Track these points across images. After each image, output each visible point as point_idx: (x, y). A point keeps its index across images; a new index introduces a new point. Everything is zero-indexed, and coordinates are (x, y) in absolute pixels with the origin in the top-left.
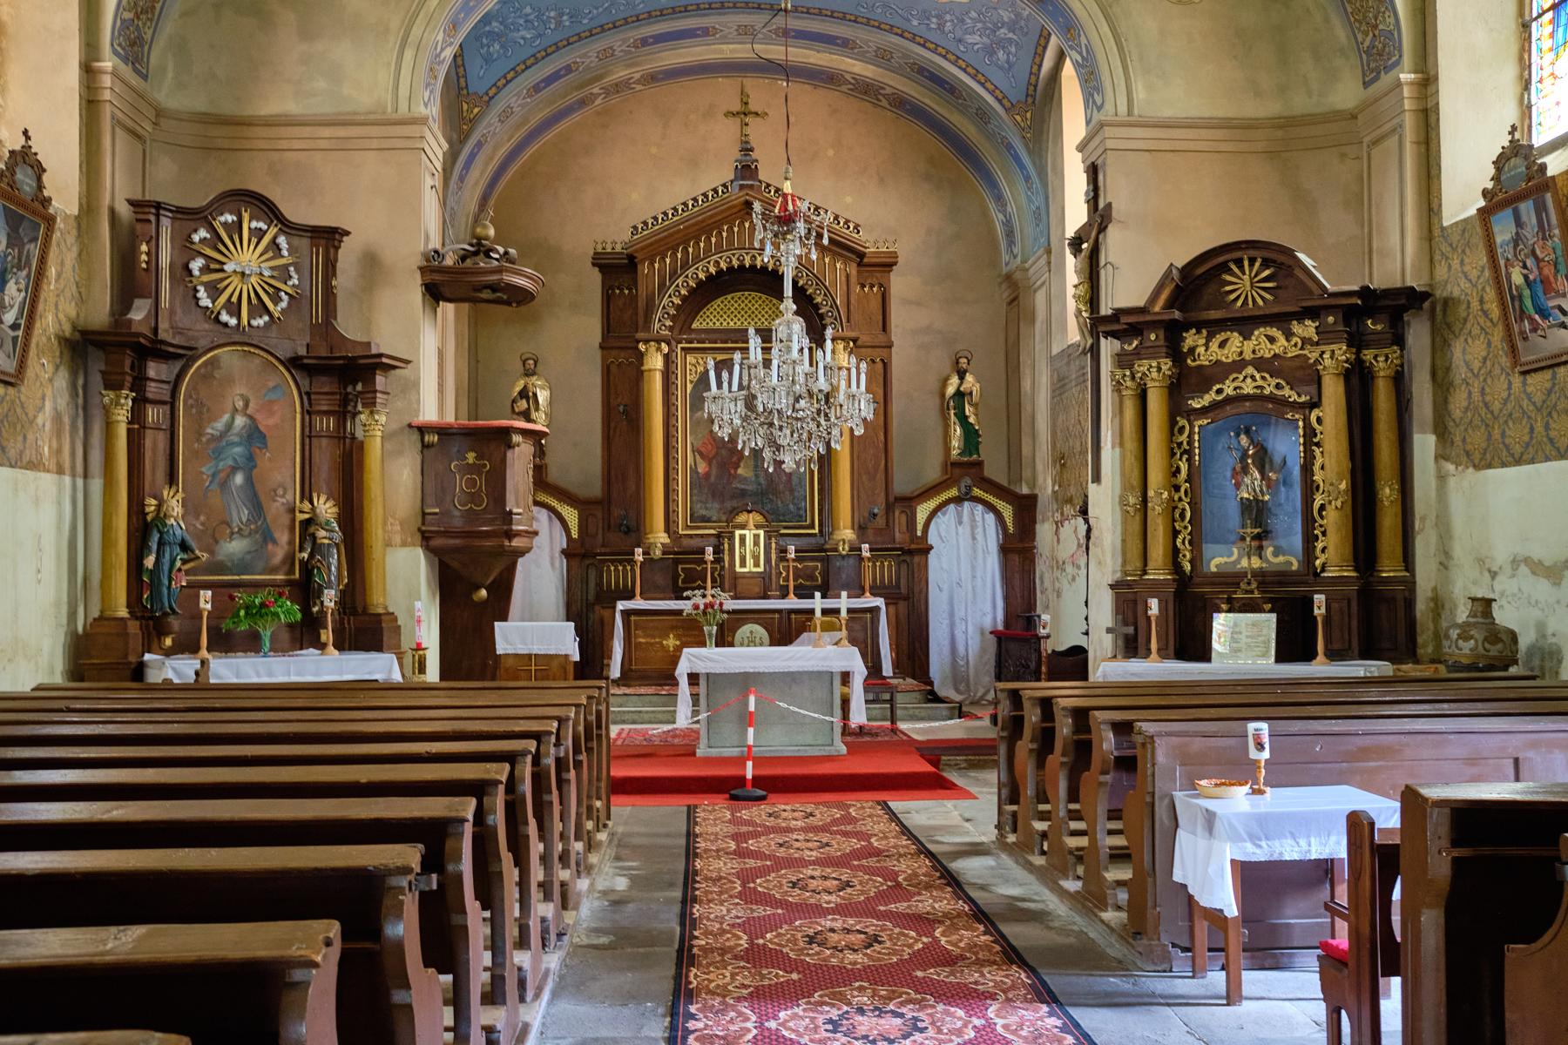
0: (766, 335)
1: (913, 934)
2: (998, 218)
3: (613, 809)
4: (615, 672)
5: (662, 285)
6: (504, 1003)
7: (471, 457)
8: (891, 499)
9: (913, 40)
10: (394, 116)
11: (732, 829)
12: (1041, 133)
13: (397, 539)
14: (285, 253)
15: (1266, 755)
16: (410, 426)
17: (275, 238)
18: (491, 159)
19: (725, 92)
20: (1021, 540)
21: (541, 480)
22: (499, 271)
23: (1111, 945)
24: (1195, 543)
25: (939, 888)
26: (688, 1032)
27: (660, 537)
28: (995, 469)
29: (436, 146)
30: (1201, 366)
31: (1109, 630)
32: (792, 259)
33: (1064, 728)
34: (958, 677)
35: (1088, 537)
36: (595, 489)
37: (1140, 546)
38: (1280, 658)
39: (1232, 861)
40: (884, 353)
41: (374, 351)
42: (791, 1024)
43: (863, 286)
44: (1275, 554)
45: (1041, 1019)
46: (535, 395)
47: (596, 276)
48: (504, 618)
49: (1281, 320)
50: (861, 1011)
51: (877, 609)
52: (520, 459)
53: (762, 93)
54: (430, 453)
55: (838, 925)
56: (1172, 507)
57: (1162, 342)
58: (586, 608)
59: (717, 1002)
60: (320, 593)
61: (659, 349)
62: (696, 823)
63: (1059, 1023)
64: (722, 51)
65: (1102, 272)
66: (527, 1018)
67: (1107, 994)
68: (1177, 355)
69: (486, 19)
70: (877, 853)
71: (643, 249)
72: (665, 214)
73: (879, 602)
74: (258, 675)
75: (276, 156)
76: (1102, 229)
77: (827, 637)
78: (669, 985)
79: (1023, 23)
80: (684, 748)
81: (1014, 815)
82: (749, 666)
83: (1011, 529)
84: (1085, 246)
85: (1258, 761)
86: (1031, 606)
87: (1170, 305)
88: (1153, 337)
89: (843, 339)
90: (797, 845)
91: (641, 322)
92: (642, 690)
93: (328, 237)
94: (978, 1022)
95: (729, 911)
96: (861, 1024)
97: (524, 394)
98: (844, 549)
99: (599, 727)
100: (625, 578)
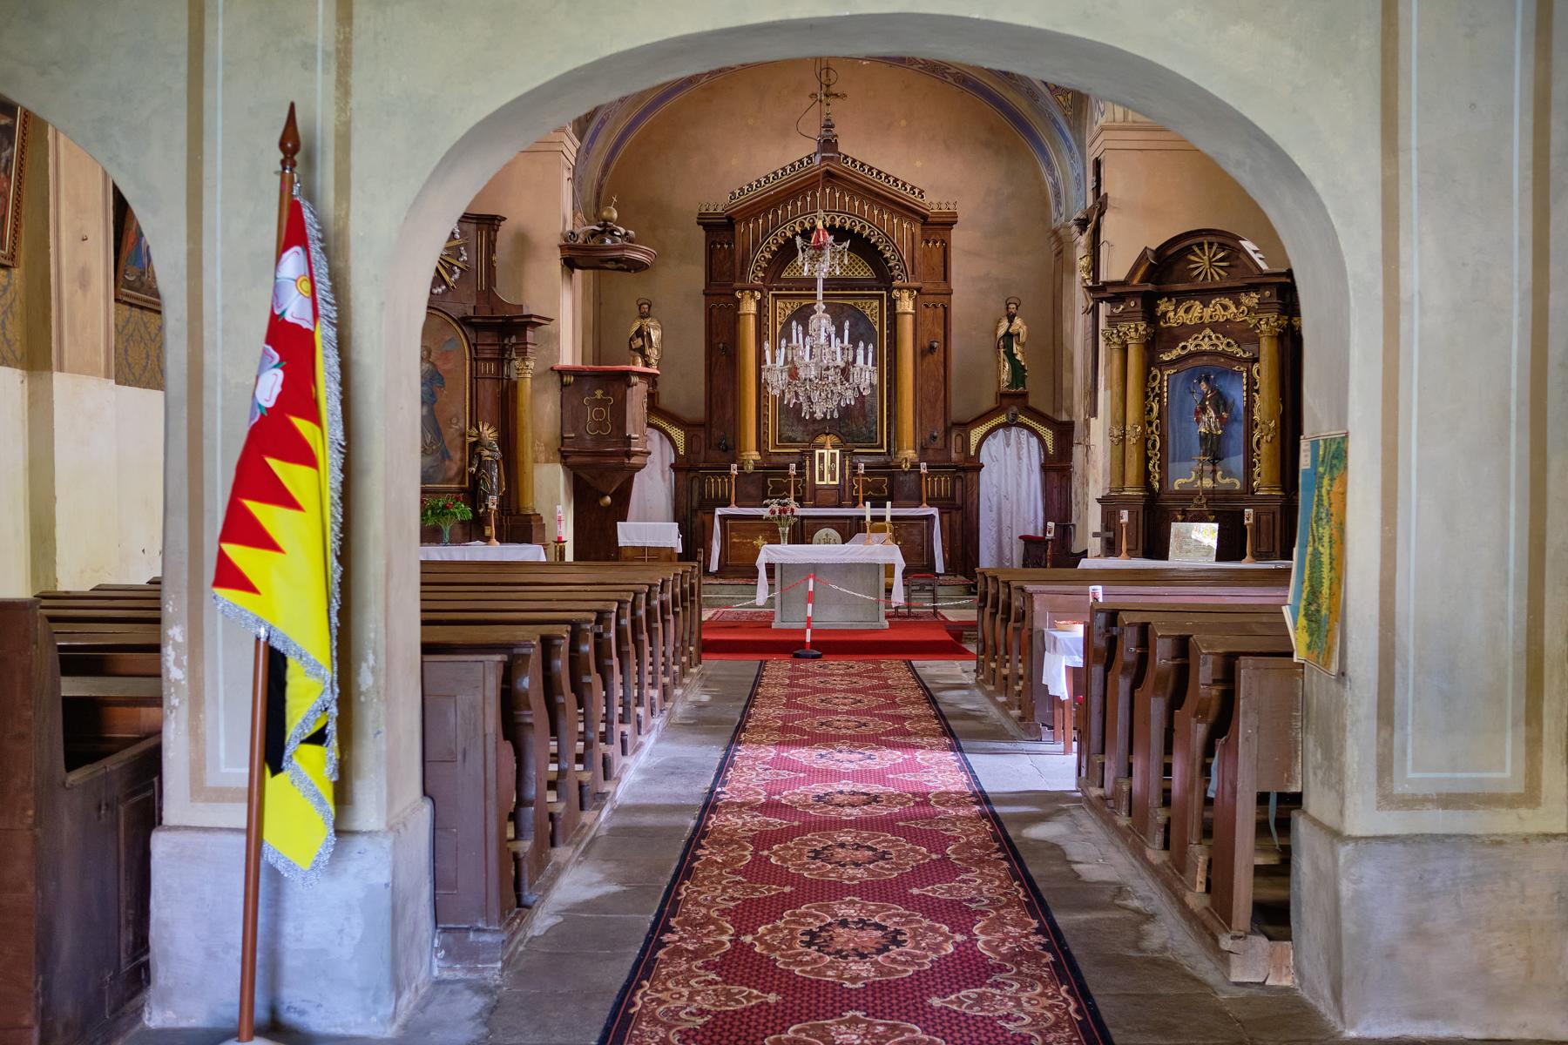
2: (1049, 180)
4: (714, 567)
5: (756, 242)
7: (599, 393)
12: (1080, 111)
13: (542, 457)
20: (1060, 460)
21: (654, 407)
22: (622, 248)
24: (1163, 467)
27: (752, 455)
33: (1205, 673)
36: (699, 413)
38: (1219, 558)
40: (944, 299)
44: (1223, 477)
47: (700, 233)
49: (1232, 292)
51: (932, 517)
52: (637, 395)
56: (1144, 440)
57: (1139, 308)
58: (691, 514)
60: (485, 496)
61: (753, 296)
68: (1151, 317)
70: (889, 687)
73: (934, 511)
76: (1101, 214)
77: (875, 536)
82: (823, 559)
87: (1144, 280)
97: (639, 333)
98: (906, 467)
99: (692, 594)
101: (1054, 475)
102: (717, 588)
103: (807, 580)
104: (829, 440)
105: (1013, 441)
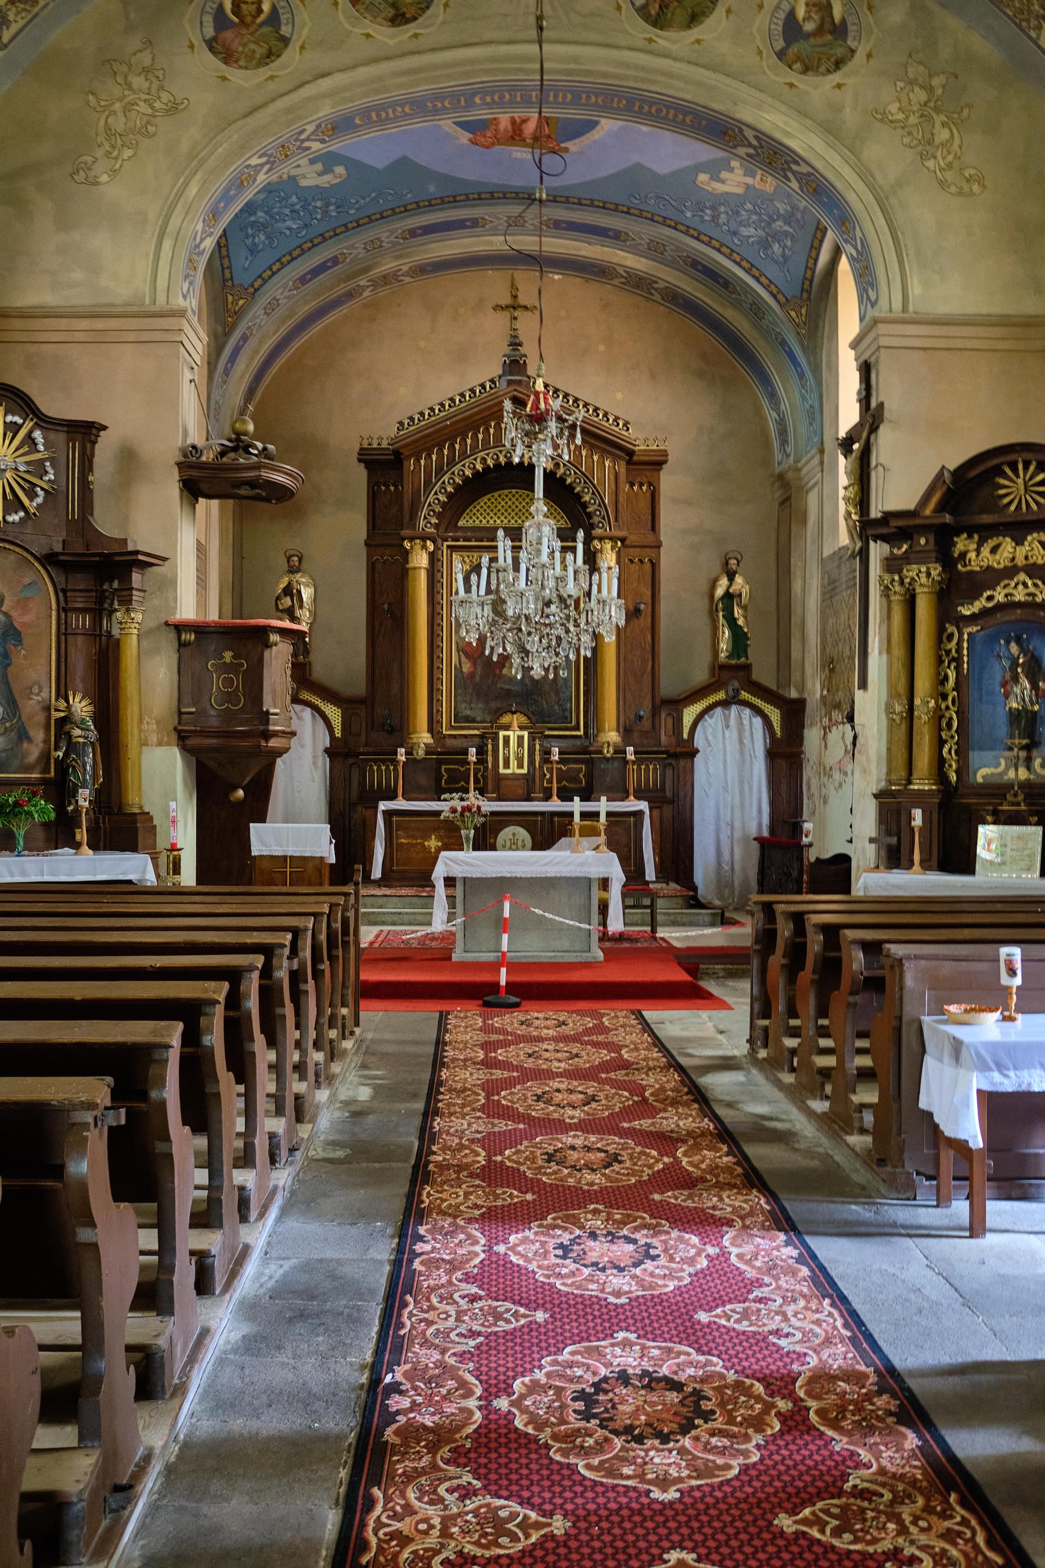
0: (515, 534)
1: (654, 1153)
2: (771, 416)
3: (362, 1014)
4: (377, 873)
5: (428, 483)
6: (221, 1227)
7: (228, 656)
8: (658, 702)
9: (686, 233)
10: (152, 308)
11: (482, 1037)
12: (817, 327)
13: (154, 738)
14: (41, 448)
15: (1018, 981)
16: (167, 624)
17: (31, 432)
18: (257, 352)
19: (495, 285)
21: (302, 674)
22: (258, 467)
23: (857, 1170)
25: (686, 1104)
26: (416, 1255)
27: (423, 738)
28: (764, 673)
29: (196, 340)
30: (972, 572)
31: (872, 840)
32: (543, 459)
33: (815, 943)
34: (723, 882)
35: (854, 744)
36: (360, 688)
37: (905, 755)
39: (979, 1091)
40: (652, 553)
41: (130, 548)
42: (520, 1249)
43: (632, 485)
45: (777, 1248)
46: (299, 592)
47: (361, 473)
48: (262, 819)
50: (593, 1236)
52: (278, 658)
53: (527, 282)
54: (186, 651)
55: (579, 1142)
56: (938, 715)
57: (932, 546)
59: (446, 1223)
61: (424, 547)
62: (447, 1031)
63: (795, 1253)
64: (491, 243)
65: (873, 474)
66: (249, 1240)
67: (847, 1223)
68: (947, 559)
69: (250, 208)
70: (626, 1065)
71: (408, 445)
72: (432, 409)
73: (643, 806)
74: (12, 875)
75: (33, 348)
76: (874, 429)
77: (586, 842)
78: (400, 1204)
79: (799, 216)
80: (438, 952)
81: (766, 1030)
82: (505, 871)
83: (779, 734)
84: (856, 446)
85: (1009, 988)
86: (798, 810)
87: (941, 508)
88: (923, 541)
89: (611, 539)
90: (547, 1055)
91: (406, 519)
92: (403, 892)
93: (85, 433)
94: (711, 1250)
95: (469, 1125)
96: (592, 1250)
97: (288, 591)
99: (345, 931)
100: (388, 780)
101: (783, 763)
102: (381, 901)
103: (500, 903)
104: (516, 719)
105: (733, 721)
